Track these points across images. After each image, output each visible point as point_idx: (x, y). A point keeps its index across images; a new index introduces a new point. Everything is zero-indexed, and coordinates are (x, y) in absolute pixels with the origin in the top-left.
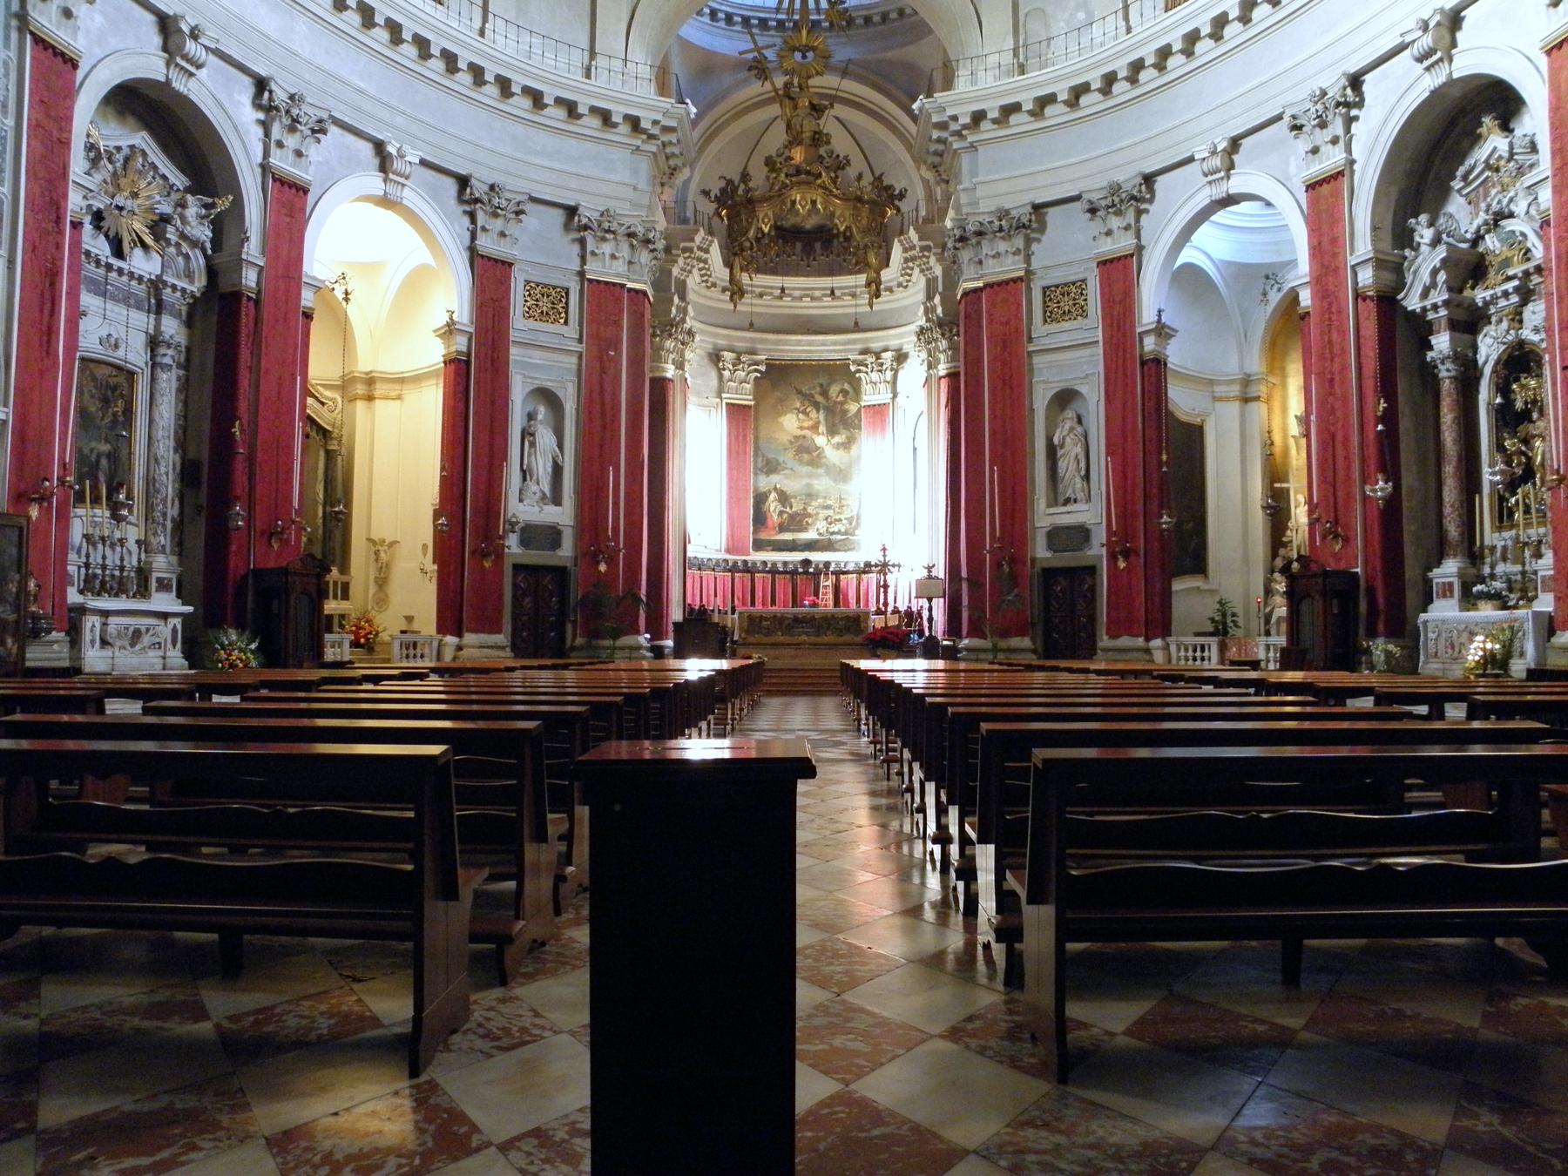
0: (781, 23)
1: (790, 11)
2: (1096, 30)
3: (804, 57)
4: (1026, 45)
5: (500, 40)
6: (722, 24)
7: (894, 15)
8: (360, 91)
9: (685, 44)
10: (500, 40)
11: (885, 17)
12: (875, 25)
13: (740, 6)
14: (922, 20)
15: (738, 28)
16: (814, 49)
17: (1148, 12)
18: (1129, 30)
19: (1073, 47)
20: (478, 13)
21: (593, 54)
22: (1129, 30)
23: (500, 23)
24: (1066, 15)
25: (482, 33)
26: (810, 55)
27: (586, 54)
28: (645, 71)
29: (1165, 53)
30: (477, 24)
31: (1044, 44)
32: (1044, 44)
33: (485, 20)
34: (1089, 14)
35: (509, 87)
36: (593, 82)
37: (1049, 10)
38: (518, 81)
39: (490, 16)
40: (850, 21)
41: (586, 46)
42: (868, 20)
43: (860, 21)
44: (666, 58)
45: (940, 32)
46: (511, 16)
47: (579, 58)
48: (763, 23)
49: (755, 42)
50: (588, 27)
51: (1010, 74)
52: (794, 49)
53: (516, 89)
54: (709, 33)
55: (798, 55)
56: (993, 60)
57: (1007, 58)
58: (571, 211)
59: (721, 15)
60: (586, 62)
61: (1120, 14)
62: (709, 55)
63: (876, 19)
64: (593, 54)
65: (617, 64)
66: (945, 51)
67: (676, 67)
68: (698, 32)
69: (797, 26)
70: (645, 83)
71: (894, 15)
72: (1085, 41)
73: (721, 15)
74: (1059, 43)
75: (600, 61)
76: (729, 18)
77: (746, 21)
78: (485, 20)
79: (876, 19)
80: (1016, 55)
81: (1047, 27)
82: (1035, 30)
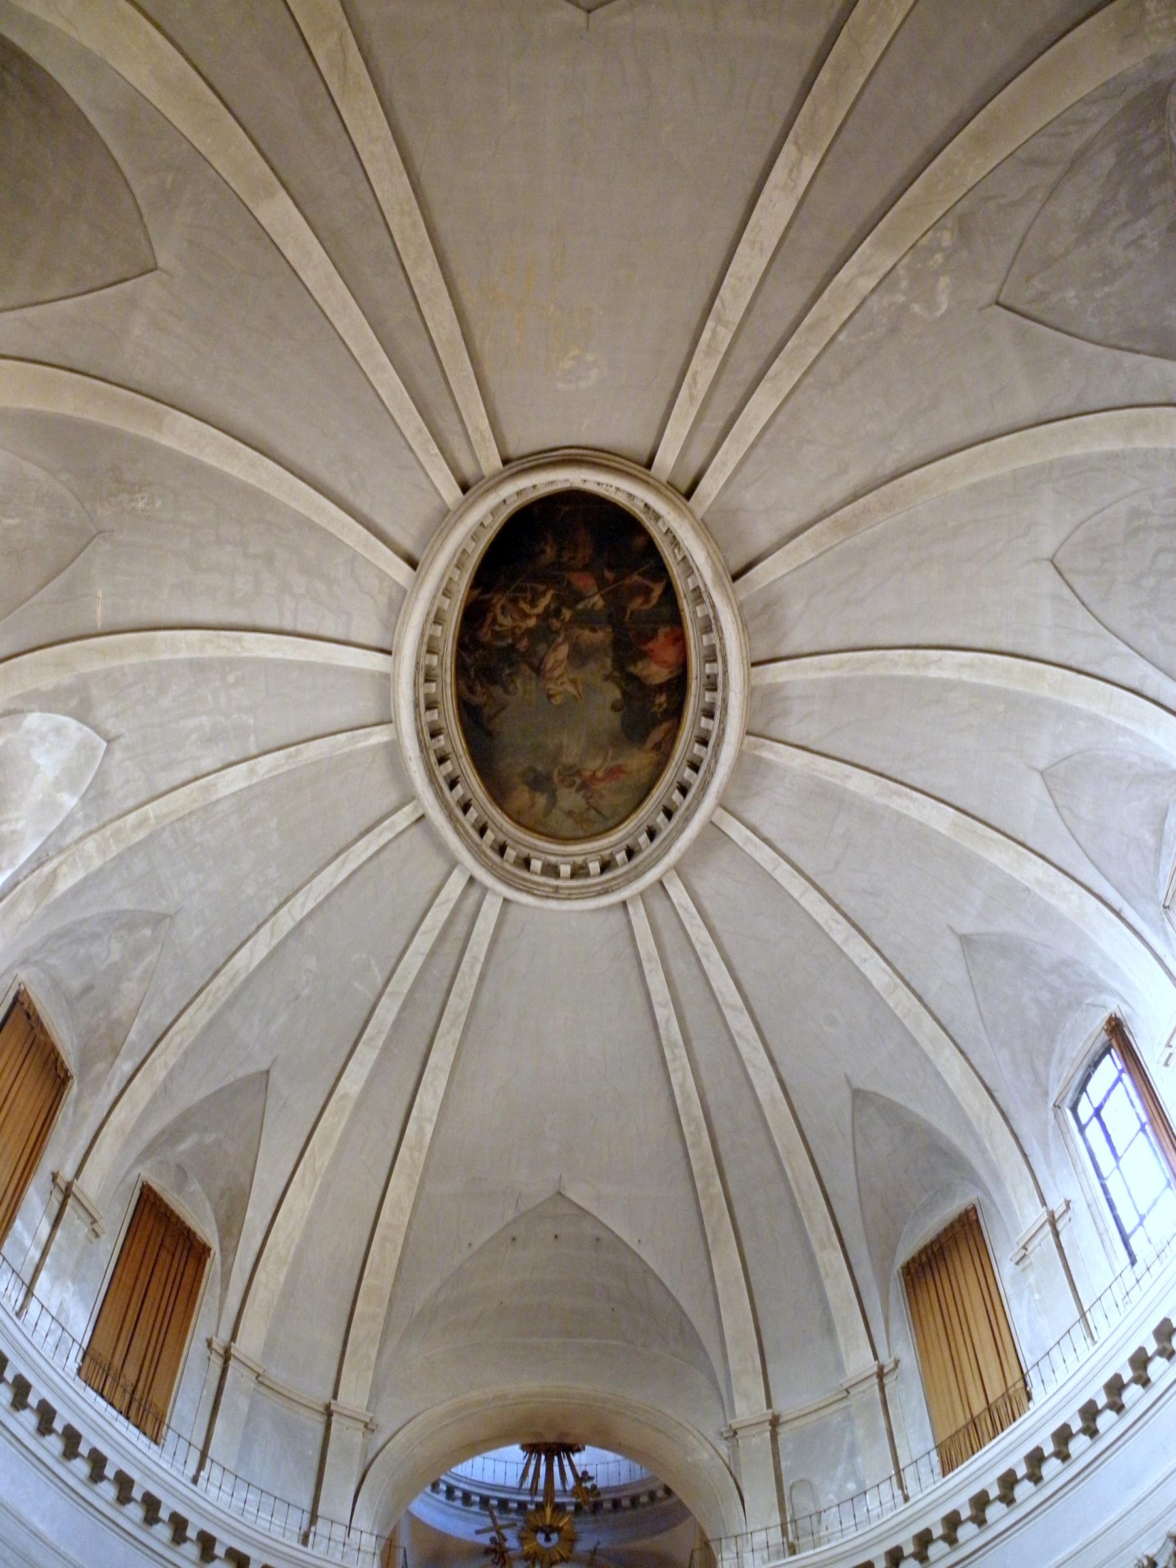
0: (522, 1506)
1: (533, 1490)
2: (871, 1500)
3: (548, 1539)
4: (794, 1521)
5: (213, 1491)
6: (458, 1503)
7: (644, 1499)
8: (36, 1535)
9: (415, 1521)
10: (213, 1491)
11: (634, 1501)
12: (625, 1509)
13: (480, 1484)
14: (680, 1503)
15: (476, 1509)
16: (558, 1530)
17: (926, 1478)
18: (906, 1499)
19: (849, 1522)
20: (195, 1457)
21: (314, 1518)
22: (906, 1499)
23: (216, 1472)
24: (834, 1487)
25: (195, 1480)
26: (554, 1537)
27: (307, 1516)
28: (369, 1542)
29: (953, 1522)
30: (191, 1470)
31: (814, 1519)
32: (814, 1519)
33: (201, 1467)
34: (860, 1483)
35: (212, 1547)
36: (309, 1549)
37: (816, 1481)
38: (225, 1541)
39: (208, 1462)
40: (596, 1507)
41: (307, 1504)
42: (616, 1504)
43: (607, 1505)
44: (395, 1531)
45: (698, 1510)
46: (231, 1465)
47: (298, 1520)
48: (503, 1504)
49: (494, 1519)
50: (312, 1487)
51: (778, 1555)
52: (536, 1530)
53: (219, 1551)
54: (445, 1513)
55: (541, 1537)
56: (759, 1538)
57: (776, 1536)
58: (259, 1375)
59: (458, 1494)
60: (305, 1527)
61: (894, 1479)
62: (444, 1537)
63: (626, 1503)
64: (314, 1518)
65: (339, 1532)
66: (703, 1533)
67: (404, 1541)
68: (430, 1510)
69: (540, 1507)
70: (369, 1558)
71: (644, 1499)
72: (861, 1513)
73: (458, 1494)
74: (831, 1517)
75: (321, 1527)
76: (466, 1498)
77: (484, 1501)
78: (201, 1467)
79: (626, 1503)
80: (784, 1533)
81: (815, 1499)
82: (802, 1503)
